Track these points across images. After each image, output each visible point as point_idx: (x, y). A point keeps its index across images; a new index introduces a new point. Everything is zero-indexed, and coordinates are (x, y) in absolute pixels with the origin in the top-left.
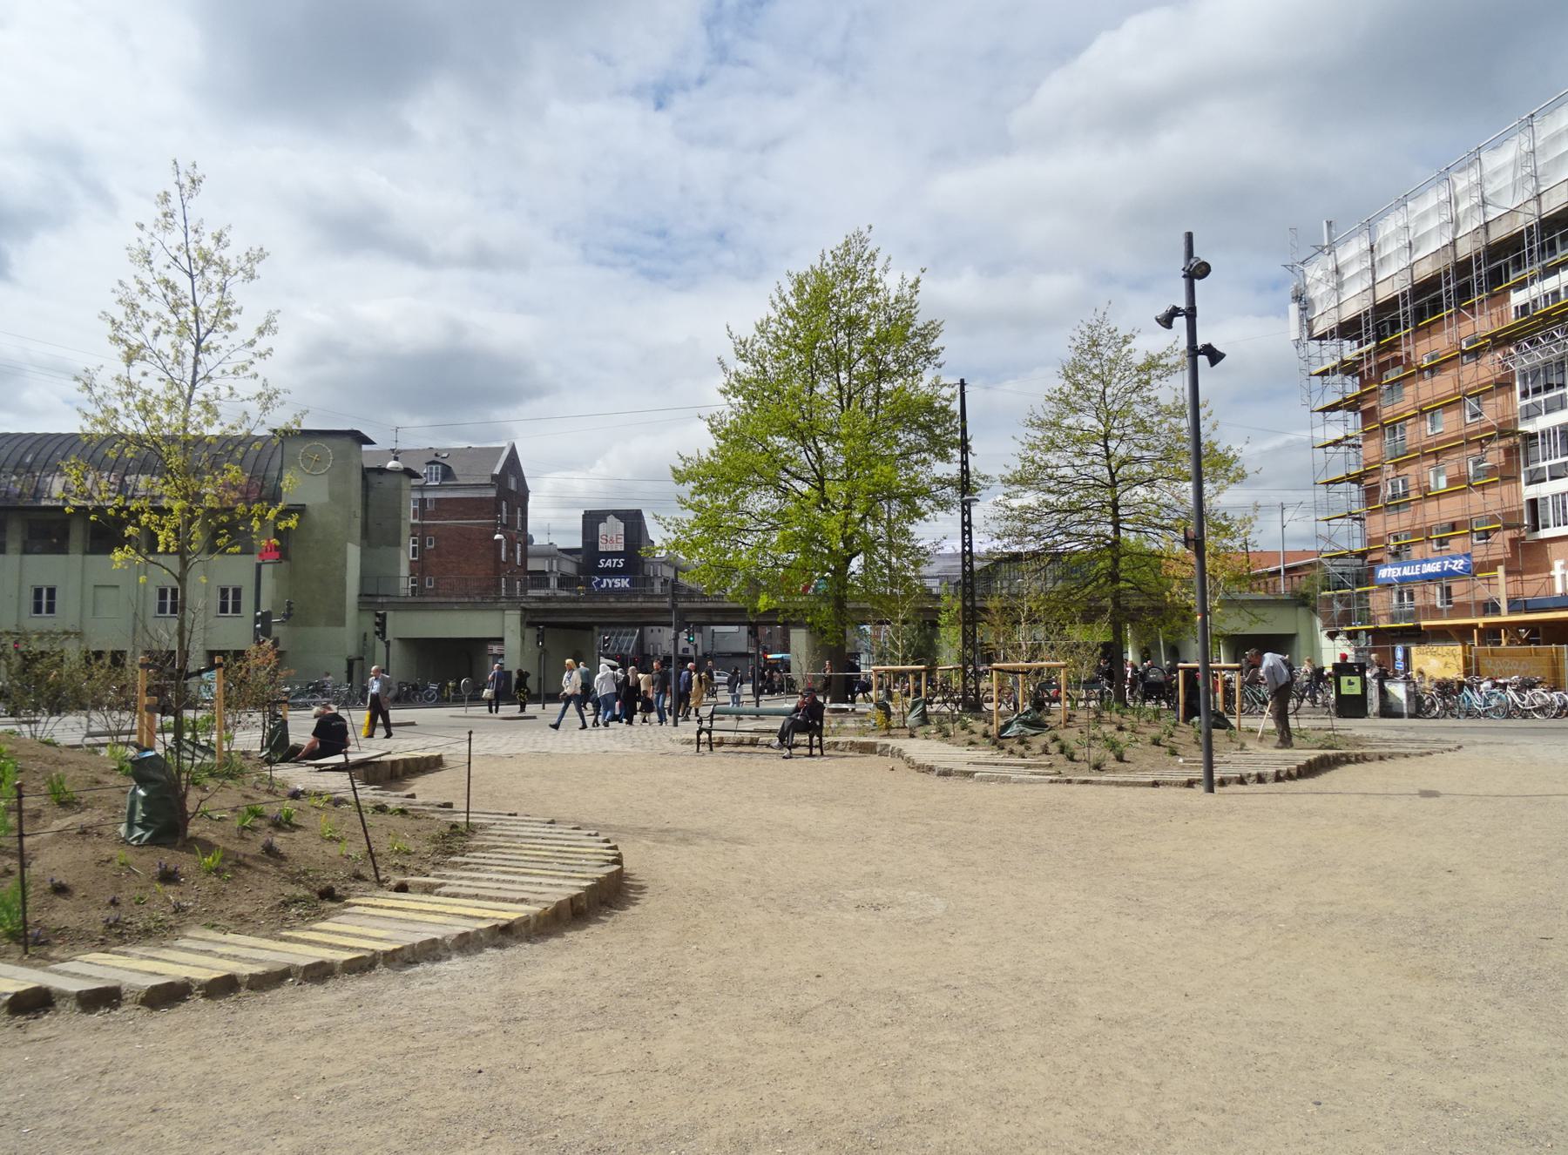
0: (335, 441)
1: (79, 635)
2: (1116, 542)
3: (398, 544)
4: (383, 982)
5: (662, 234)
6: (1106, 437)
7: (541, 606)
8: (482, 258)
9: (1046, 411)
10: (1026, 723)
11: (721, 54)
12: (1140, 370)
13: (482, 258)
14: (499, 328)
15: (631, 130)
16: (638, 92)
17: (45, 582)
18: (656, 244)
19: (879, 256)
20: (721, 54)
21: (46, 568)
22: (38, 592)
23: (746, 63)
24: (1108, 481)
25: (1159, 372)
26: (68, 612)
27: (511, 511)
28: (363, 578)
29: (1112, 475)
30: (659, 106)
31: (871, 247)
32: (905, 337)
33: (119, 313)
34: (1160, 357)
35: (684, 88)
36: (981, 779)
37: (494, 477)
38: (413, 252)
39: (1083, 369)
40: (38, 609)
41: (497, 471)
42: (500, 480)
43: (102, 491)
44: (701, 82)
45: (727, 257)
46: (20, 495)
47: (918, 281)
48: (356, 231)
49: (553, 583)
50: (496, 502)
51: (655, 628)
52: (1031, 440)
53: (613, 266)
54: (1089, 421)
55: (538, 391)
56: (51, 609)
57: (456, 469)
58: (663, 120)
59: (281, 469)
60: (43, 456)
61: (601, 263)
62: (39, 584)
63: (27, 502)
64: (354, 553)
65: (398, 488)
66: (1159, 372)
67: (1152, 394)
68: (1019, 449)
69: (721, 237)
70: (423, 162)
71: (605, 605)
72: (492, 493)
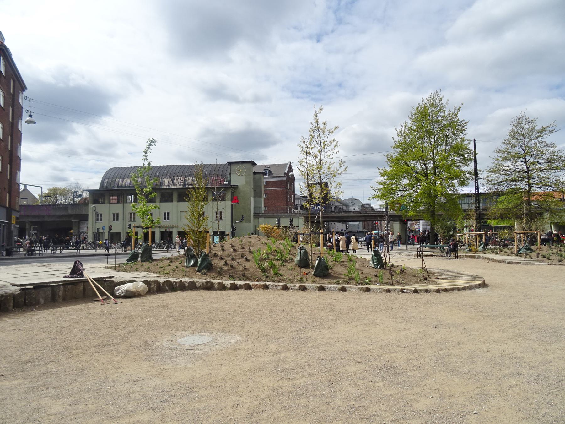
0: (246, 165)
1: (177, 227)
2: (529, 191)
3: (261, 197)
4: (456, 294)
5: (319, 86)
6: (525, 156)
7: (358, 215)
8: (257, 99)
9: (504, 147)
10: (526, 249)
11: (340, 21)
12: (538, 132)
13: (257, 99)
14: (263, 123)
15: (309, 51)
16: (310, 37)
17: (167, 211)
18: (317, 89)
19: (443, 99)
20: (340, 21)
21: (166, 207)
22: (165, 214)
23: (348, 23)
24: (526, 170)
25: (546, 133)
26: (173, 220)
27: (290, 186)
28: (254, 208)
29: (528, 168)
30: (318, 41)
31: (441, 96)
32: (455, 126)
33: (496, 162)
34: (546, 127)
35: (327, 34)
36: (523, 264)
37: (285, 174)
38: (234, 99)
39: (517, 133)
40: (165, 219)
41: (286, 172)
42: (287, 174)
43: (178, 183)
44: (333, 31)
45: (342, 92)
46: (157, 185)
47: (460, 107)
48: (217, 93)
49: (299, 208)
50: (286, 181)
51: (333, 223)
52: (497, 157)
53: (302, 98)
54: (518, 150)
55: (274, 143)
56: (168, 219)
57: (273, 172)
58: (320, 46)
59: (230, 174)
60: (162, 173)
61: (298, 98)
62: (165, 211)
63: (158, 187)
64: (252, 199)
65: (261, 179)
66: (546, 133)
67: (543, 140)
68: (493, 161)
69: (340, 85)
70: (237, 68)
71: (331, 215)
72: (285, 179)
